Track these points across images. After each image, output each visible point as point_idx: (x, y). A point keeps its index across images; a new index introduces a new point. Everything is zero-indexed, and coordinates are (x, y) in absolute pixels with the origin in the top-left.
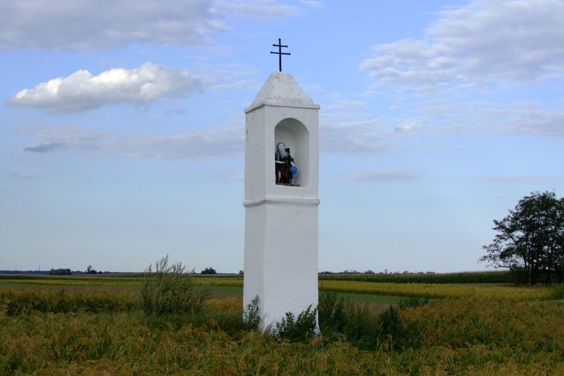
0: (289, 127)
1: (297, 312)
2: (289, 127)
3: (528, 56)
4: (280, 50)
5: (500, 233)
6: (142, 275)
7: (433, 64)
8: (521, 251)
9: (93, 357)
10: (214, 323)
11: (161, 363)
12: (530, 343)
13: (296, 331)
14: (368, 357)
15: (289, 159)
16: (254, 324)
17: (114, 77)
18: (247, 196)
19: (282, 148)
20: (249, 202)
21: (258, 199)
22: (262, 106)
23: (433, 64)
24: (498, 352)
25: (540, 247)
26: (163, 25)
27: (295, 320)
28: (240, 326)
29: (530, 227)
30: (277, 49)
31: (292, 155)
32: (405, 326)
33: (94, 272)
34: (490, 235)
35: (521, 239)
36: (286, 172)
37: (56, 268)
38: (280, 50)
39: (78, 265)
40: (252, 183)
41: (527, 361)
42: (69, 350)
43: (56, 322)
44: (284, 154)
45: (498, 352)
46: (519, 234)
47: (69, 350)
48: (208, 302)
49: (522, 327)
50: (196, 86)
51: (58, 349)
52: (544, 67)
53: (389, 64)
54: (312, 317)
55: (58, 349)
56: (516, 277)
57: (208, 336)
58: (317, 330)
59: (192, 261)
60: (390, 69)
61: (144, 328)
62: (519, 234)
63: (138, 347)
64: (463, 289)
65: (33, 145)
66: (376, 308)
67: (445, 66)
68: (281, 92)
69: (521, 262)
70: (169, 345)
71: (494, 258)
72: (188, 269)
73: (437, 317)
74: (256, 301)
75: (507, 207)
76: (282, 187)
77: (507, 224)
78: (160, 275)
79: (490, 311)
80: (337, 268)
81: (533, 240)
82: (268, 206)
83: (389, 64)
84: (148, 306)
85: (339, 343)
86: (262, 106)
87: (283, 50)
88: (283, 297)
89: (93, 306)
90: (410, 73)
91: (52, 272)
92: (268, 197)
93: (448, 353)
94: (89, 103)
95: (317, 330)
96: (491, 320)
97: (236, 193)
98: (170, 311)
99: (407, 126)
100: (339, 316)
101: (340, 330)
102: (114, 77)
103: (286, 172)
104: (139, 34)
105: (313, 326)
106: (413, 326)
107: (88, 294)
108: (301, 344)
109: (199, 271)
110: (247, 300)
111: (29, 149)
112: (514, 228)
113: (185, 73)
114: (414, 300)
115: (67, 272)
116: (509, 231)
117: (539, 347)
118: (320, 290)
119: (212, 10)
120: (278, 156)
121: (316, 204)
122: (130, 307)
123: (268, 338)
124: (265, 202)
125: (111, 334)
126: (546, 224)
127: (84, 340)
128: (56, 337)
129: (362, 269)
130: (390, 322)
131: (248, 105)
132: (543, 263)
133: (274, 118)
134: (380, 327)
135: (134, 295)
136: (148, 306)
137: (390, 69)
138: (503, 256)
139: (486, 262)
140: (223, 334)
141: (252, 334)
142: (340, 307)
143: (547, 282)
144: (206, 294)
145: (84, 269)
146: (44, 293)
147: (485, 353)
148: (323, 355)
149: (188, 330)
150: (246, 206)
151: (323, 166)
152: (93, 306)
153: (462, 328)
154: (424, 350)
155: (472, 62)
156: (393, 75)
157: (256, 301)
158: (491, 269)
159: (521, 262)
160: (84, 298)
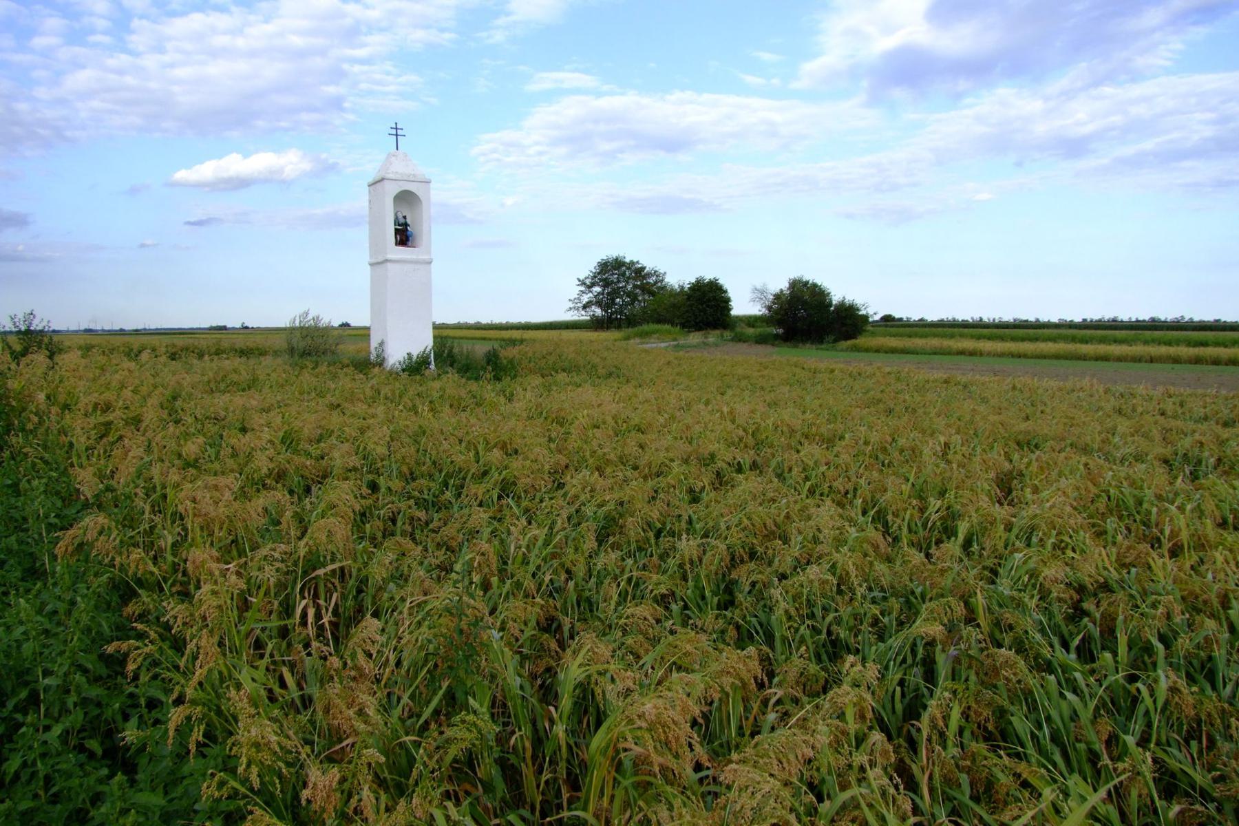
0: (406, 198)
1: (416, 351)
2: (406, 198)
3: (606, 147)
4: (397, 132)
5: (583, 288)
6: (284, 329)
7: (531, 151)
8: (599, 303)
9: (244, 390)
10: (346, 361)
11: (301, 393)
12: (601, 371)
13: (415, 367)
14: (473, 386)
15: (406, 225)
16: (381, 362)
17: (259, 162)
18: (371, 256)
19: (400, 216)
20: (374, 261)
21: (380, 259)
22: (383, 179)
23: (531, 151)
24: (577, 379)
25: (613, 300)
26: (305, 117)
27: (415, 358)
28: (367, 364)
29: (606, 283)
30: (394, 132)
31: (409, 221)
32: (505, 362)
33: (247, 328)
34: (575, 290)
35: (599, 293)
36: (404, 236)
37: (214, 325)
38: (397, 132)
39: (233, 322)
40: (375, 245)
41: (599, 385)
42: (222, 386)
43: (210, 366)
44: (402, 221)
45: (577, 379)
46: (597, 289)
47: (222, 386)
48: (341, 347)
49: (596, 360)
50: (332, 168)
51: (213, 385)
52: (620, 156)
53: (494, 151)
54: (428, 356)
55: (213, 385)
56: (597, 324)
57: (341, 373)
58: (433, 366)
59: (332, 316)
60: (495, 156)
61: (286, 367)
62: (597, 289)
63: (280, 380)
64: (554, 334)
65: (192, 220)
66: (481, 349)
67: (540, 153)
68: (398, 168)
69: (598, 312)
70: (307, 378)
71: (578, 309)
72: (324, 322)
73: (530, 354)
74: (381, 344)
75: (587, 267)
76: (401, 248)
77: (588, 282)
78: (301, 328)
79: (572, 349)
80: (451, 320)
81: (608, 294)
82: (389, 265)
83: (494, 151)
84: (292, 351)
85: (450, 375)
86: (383, 179)
87: (400, 132)
88: (404, 341)
89: (244, 353)
90: (511, 159)
91: (211, 328)
92: (389, 256)
93: (538, 380)
94: (240, 183)
95: (433, 366)
96: (573, 355)
97: (363, 257)
98: (309, 354)
99: (510, 201)
100: (451, 355)
101: (452, 365)
102: (259, 162)
103: (404, 236)
104: (283, 124)
105: (429, 364)
106: (511, 361)
107: (240, 342)
108: (418, 377)
109: (336, 324)
110: (374, 343)
111: (189, 223)
112: (593, 285)
113: (324, 156)
114: (512, 342)
115: (224, 328)
116: (590, 287)
117: (610, 374)
118: (435, 337)
119: (346, 105)
120: (396, 222)
121: (430, 263)
122: (276, 353)
123: (393, 374)
124: (387, 261)
125: (258, 372)
126: (619, 282)
127: (235, 377)
128: (211, 374)
129: (472, 321)
130: (492, 359)
131: (371, 180)
132: (616, 312)
133: (392, 190)
134: (484, 363)
135: (280, 343)
136: (292, 351)
137: (495, 156)
138: (585, 307)
139: (571, 312)
140: (350, 370)
141: (376, 370)
142: (452, 348)
143: (619, 327)
144: (340, 340)
145: (238, 325)
146: (203, 343)
147: (567, 380)
148: (437, 385)
149: (323, 368)
150: (371, 265)
151: (435, 234)
152: (244, 353)
153: (550, 362)
154: (519, 379)
155: (563, 150)
156: (498, 160)
157: (381, 344)
158: (576, 318)
159: (598, 312)
160: (237, 347)
